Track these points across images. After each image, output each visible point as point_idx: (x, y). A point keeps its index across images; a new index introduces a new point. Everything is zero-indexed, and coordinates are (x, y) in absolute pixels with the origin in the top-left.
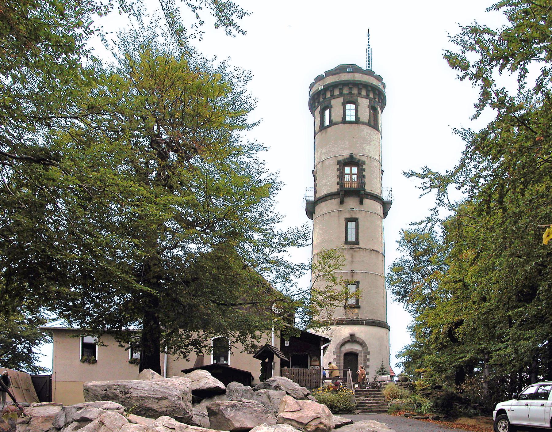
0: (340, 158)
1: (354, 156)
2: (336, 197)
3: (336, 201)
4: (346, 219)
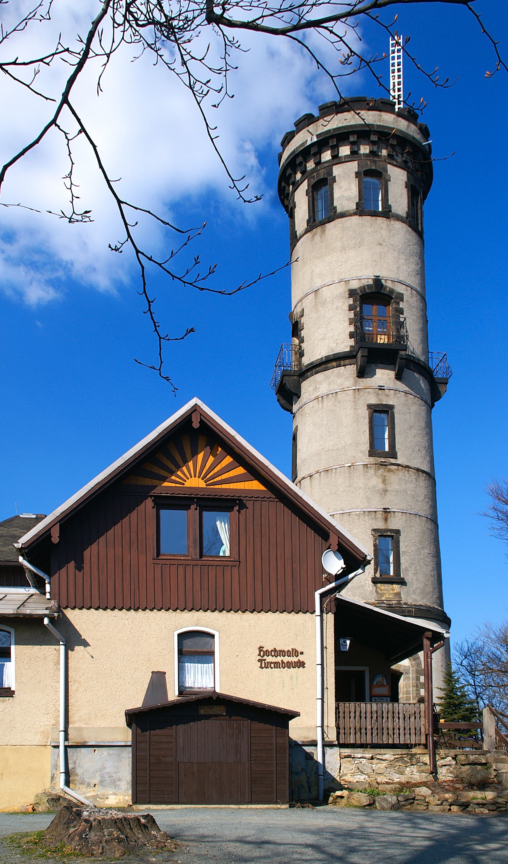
0: (355, 285)
1: (383, 281)
2: (347, 361)
3: (350, 370)
4: (369, 406)
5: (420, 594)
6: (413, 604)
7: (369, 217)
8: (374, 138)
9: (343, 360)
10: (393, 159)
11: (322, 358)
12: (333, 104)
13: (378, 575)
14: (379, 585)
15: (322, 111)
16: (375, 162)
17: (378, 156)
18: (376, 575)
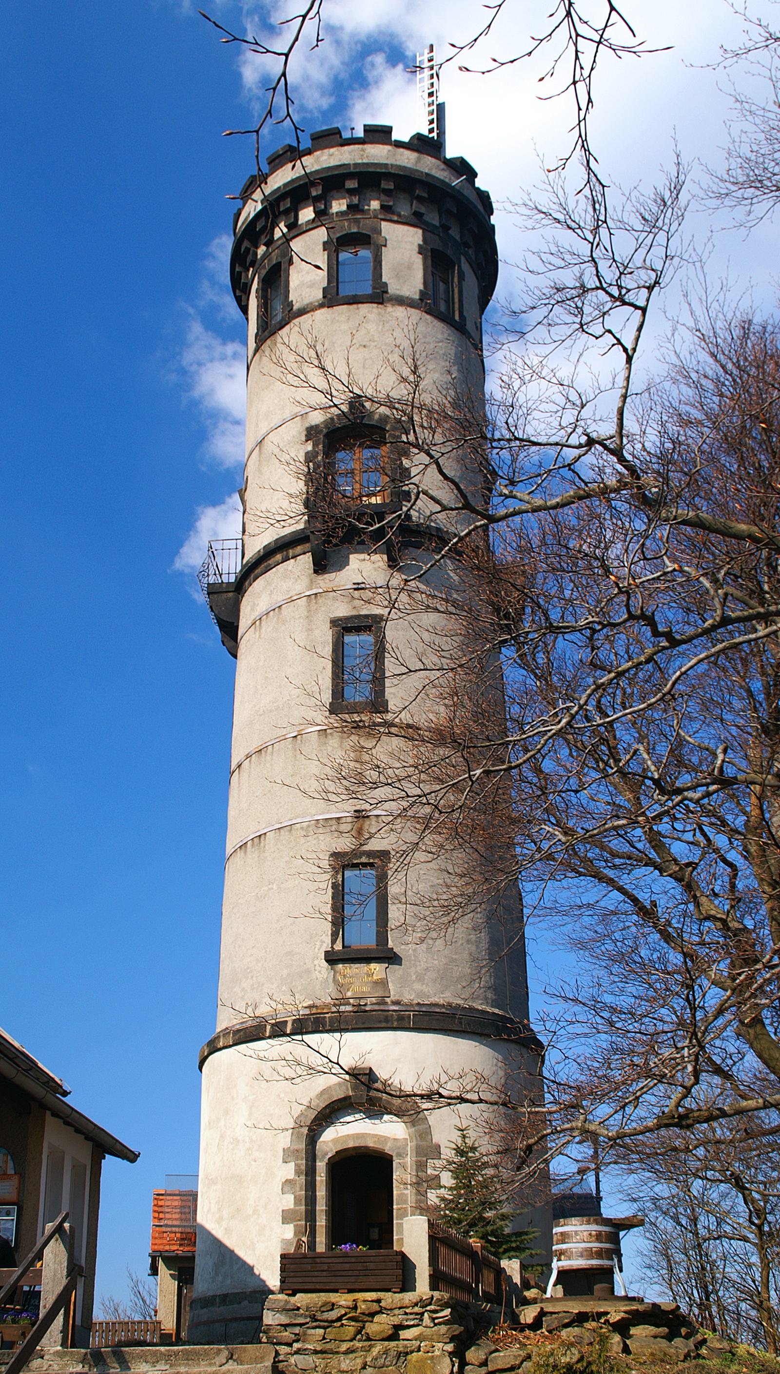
4: (334, 622)
5: (434, 981)
6: (415, 1002)
7: (345, 306)
8: (351, 184)
9: (292, 548)
10: (393, 213)
11: (259, 551)
12: (287, 148)
13: (338, 946)
14: (341, 966)
15: (273, 164)
16: (357, 221)
17: (363, 211)
18: (334, 946)
